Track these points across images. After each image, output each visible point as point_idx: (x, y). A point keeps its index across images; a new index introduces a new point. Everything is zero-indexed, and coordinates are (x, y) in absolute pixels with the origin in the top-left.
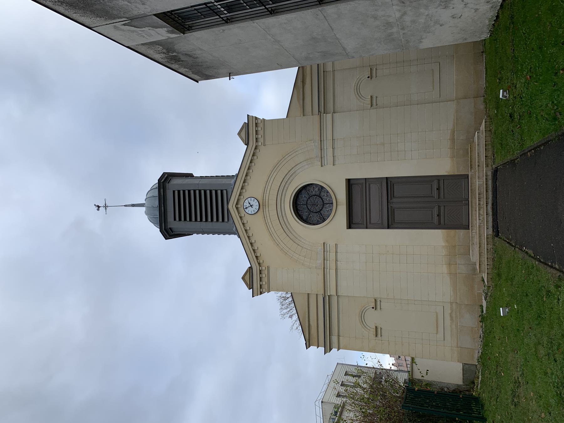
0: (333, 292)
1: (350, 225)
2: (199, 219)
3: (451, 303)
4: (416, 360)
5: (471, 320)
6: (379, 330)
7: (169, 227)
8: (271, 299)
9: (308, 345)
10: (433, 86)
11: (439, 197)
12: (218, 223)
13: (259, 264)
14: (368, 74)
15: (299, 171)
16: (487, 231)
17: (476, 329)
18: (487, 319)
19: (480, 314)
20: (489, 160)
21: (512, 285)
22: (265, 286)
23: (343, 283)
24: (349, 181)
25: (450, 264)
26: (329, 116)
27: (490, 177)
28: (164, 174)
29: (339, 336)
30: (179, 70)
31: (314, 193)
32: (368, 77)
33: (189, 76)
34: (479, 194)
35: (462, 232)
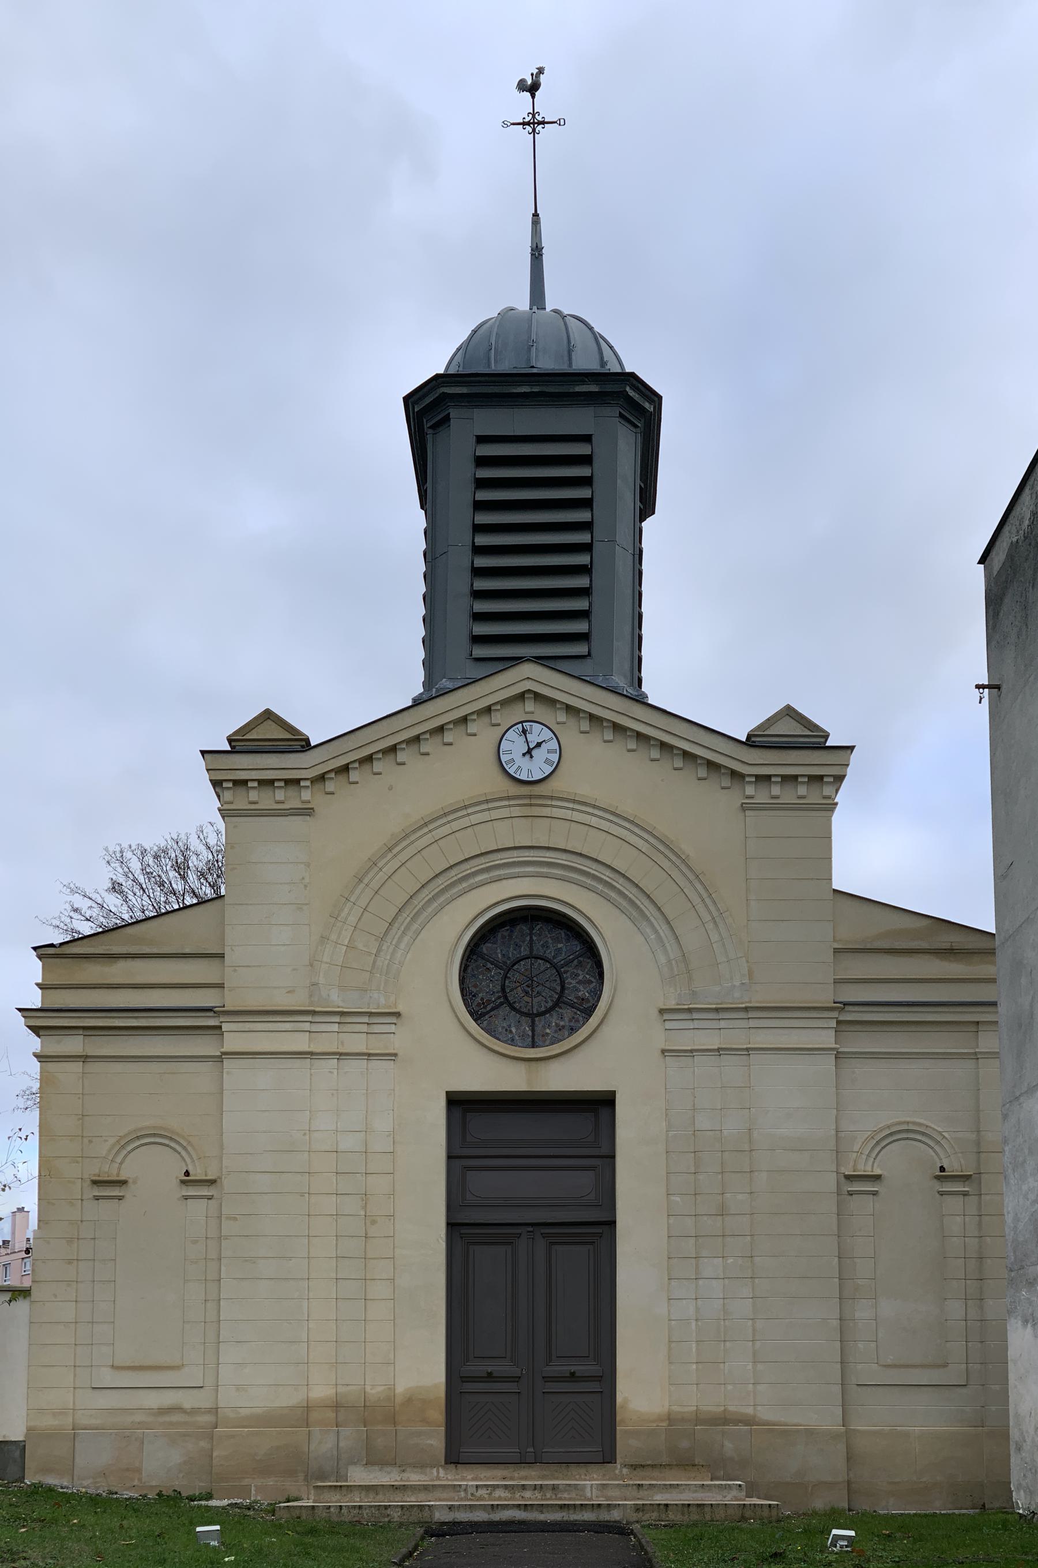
0: (233, 1041)
1: (459, 1104)
2: (482, 540)
3: (215, 1410)
4: (22, 1306)
5: (161, 1466)
6: (116, 1192)
7: (453, 413)
8: (193, 815)
9: (43, 952)
10: (895, 1366)
11: (546, 1379)
12: (465, 618)
13: (322, 778)
14: (953, 1166)
15: (648, 930)
16: (442, 1508)
17: (136, 1483)
18: (175, 1506)
19: (184, 1494)
20: (655, 1515)
21: (290, 1554)
22: (241, 800)
23: (264, 1076)
24: (602, 1104)
25: (337, 1406)
26: (827, 1039)
27: (604, 1516)
28: (656, 399)
29: (85, 1058)
30: (1027, 491)
31: (570, 982)
32: (942, 1169)
33: (1006, 529)
34: (554, 1488)
35: (436, 1442)
